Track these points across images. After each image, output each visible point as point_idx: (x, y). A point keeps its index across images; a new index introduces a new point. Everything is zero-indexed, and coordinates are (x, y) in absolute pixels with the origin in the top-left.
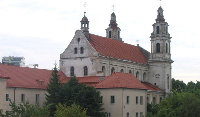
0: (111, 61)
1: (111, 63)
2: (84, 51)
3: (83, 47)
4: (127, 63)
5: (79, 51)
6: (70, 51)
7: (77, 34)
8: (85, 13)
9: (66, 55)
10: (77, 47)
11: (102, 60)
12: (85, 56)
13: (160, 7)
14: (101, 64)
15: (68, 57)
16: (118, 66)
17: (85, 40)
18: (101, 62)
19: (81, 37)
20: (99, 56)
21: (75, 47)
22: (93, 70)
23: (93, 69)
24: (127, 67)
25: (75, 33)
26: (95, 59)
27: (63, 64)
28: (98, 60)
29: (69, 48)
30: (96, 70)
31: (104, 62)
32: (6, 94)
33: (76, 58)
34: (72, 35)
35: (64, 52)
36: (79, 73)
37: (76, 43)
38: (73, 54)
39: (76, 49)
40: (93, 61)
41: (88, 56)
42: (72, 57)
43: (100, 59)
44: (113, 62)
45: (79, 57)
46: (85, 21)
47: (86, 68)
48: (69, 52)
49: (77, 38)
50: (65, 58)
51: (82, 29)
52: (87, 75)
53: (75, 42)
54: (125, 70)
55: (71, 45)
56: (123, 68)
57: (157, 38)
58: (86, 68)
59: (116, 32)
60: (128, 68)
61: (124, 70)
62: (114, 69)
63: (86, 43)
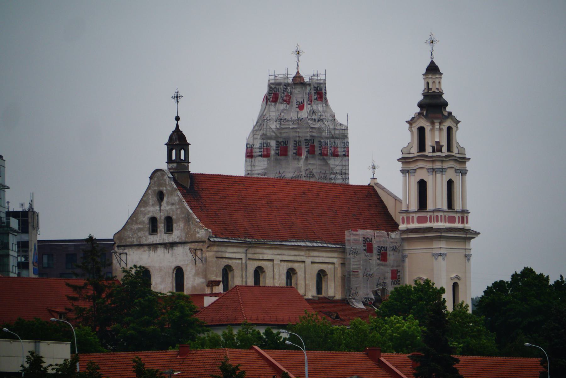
0: (250, 250)
1: (250, 256)
2: (175, 225)
3: (171, 215)
4: (309, 250)
5: (161, 227)
6: (141, 226)
7: (156, 179)
8: (177, 119)
9: (129, 237)
10: (158, 217)
11: (223, 249)
12: (177, 240)
13: (432, 63)
14: (221, 260)
15: (136, 243)
16: (275, 262)
17: (176, 198)
18: (219, 255)
19: (166, 190)
20: (212, 239)
21: (150, 215)
22: (196, 278)
23: (197, 274)
24: (308, 260)
25: (151, 178)
26: (202, 250)
27: (122, 263)
28: (208, 251)
29: (137, 219)
30: (203, 278)
31: (227, 255)
32: (467, 223)
33: (154, 246)
34: (141, 185)
35: (124, 228)
36: (162, 285)
37: (153, 205)
38: (147, 233)
39: (153, 221)
40: (196, 255)
41: (183, 239)
42: (145, 243)
43: (215, 249)
44: (258, 250)
45: (161, 242)
46: (178, 141)
47: (179, 273)
48: (137, 229)
49: (157, 191)
50: (128, 243)
51: (171, 165)
52: (321, 294)
53: (151, 202)
54: (303, 270)
55: (143, 209)
56: (295, 266)
57: (420, 164)
58: (179, 273)
59: (440, 129)
60: (313, 263)
61: (297, 271)
62: (264, 271)
63: (177, 207)
